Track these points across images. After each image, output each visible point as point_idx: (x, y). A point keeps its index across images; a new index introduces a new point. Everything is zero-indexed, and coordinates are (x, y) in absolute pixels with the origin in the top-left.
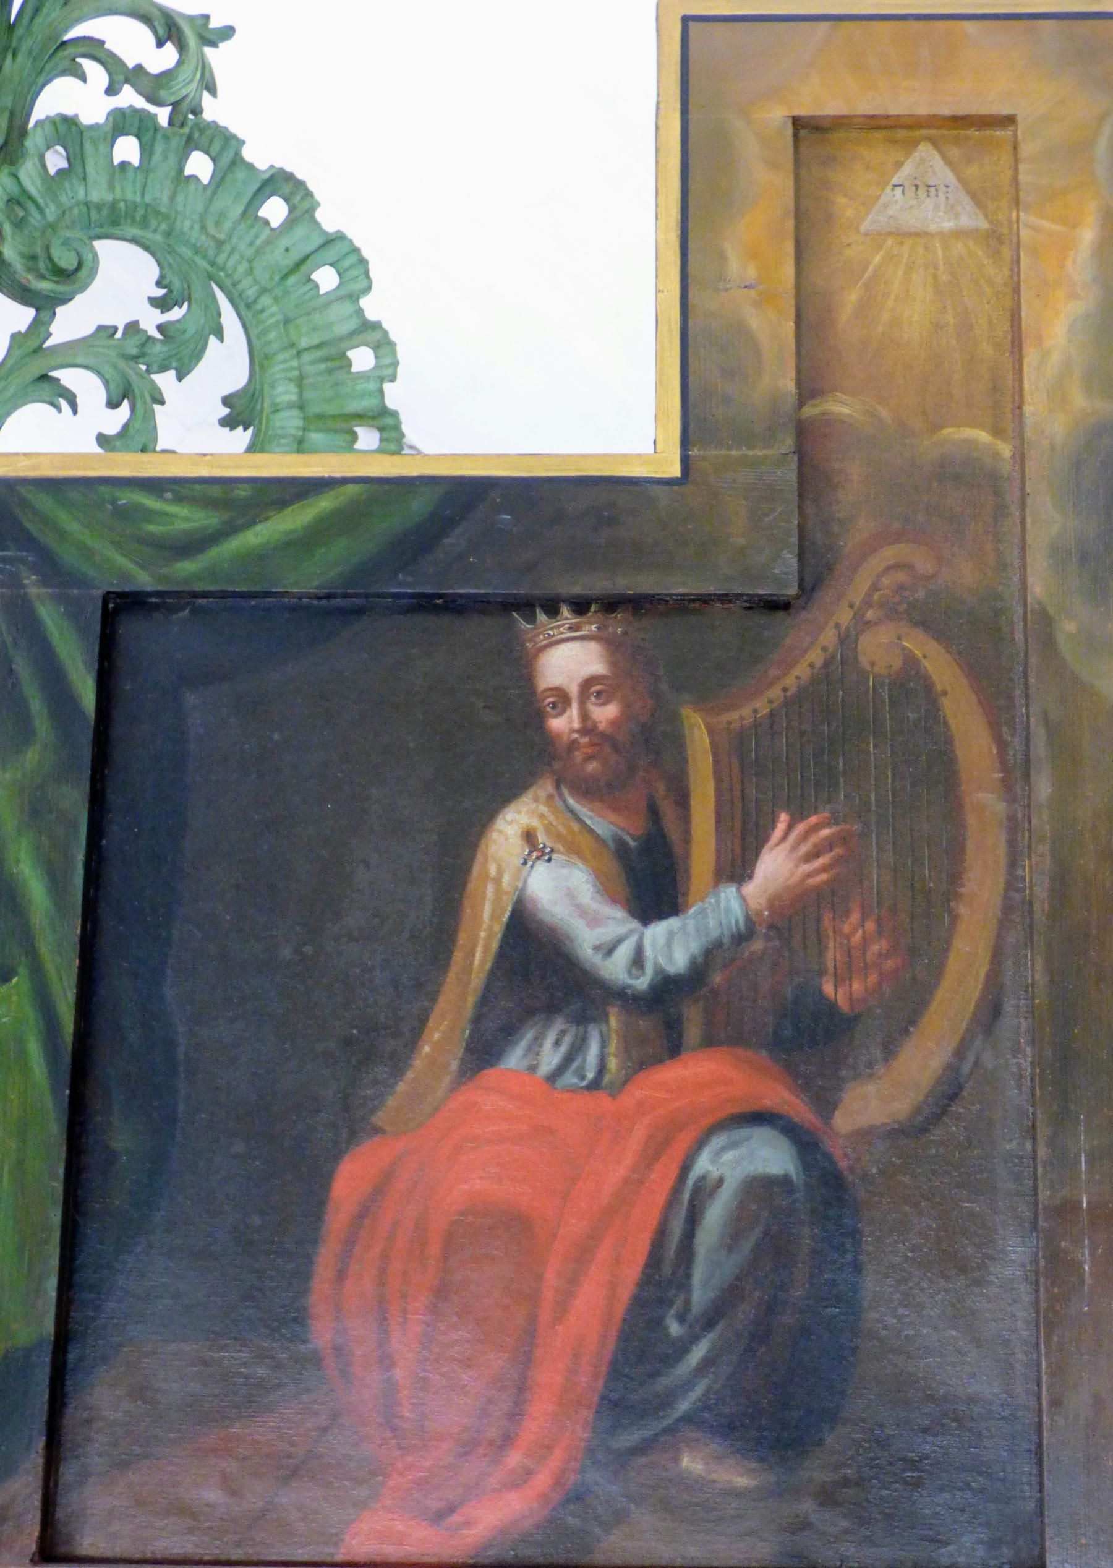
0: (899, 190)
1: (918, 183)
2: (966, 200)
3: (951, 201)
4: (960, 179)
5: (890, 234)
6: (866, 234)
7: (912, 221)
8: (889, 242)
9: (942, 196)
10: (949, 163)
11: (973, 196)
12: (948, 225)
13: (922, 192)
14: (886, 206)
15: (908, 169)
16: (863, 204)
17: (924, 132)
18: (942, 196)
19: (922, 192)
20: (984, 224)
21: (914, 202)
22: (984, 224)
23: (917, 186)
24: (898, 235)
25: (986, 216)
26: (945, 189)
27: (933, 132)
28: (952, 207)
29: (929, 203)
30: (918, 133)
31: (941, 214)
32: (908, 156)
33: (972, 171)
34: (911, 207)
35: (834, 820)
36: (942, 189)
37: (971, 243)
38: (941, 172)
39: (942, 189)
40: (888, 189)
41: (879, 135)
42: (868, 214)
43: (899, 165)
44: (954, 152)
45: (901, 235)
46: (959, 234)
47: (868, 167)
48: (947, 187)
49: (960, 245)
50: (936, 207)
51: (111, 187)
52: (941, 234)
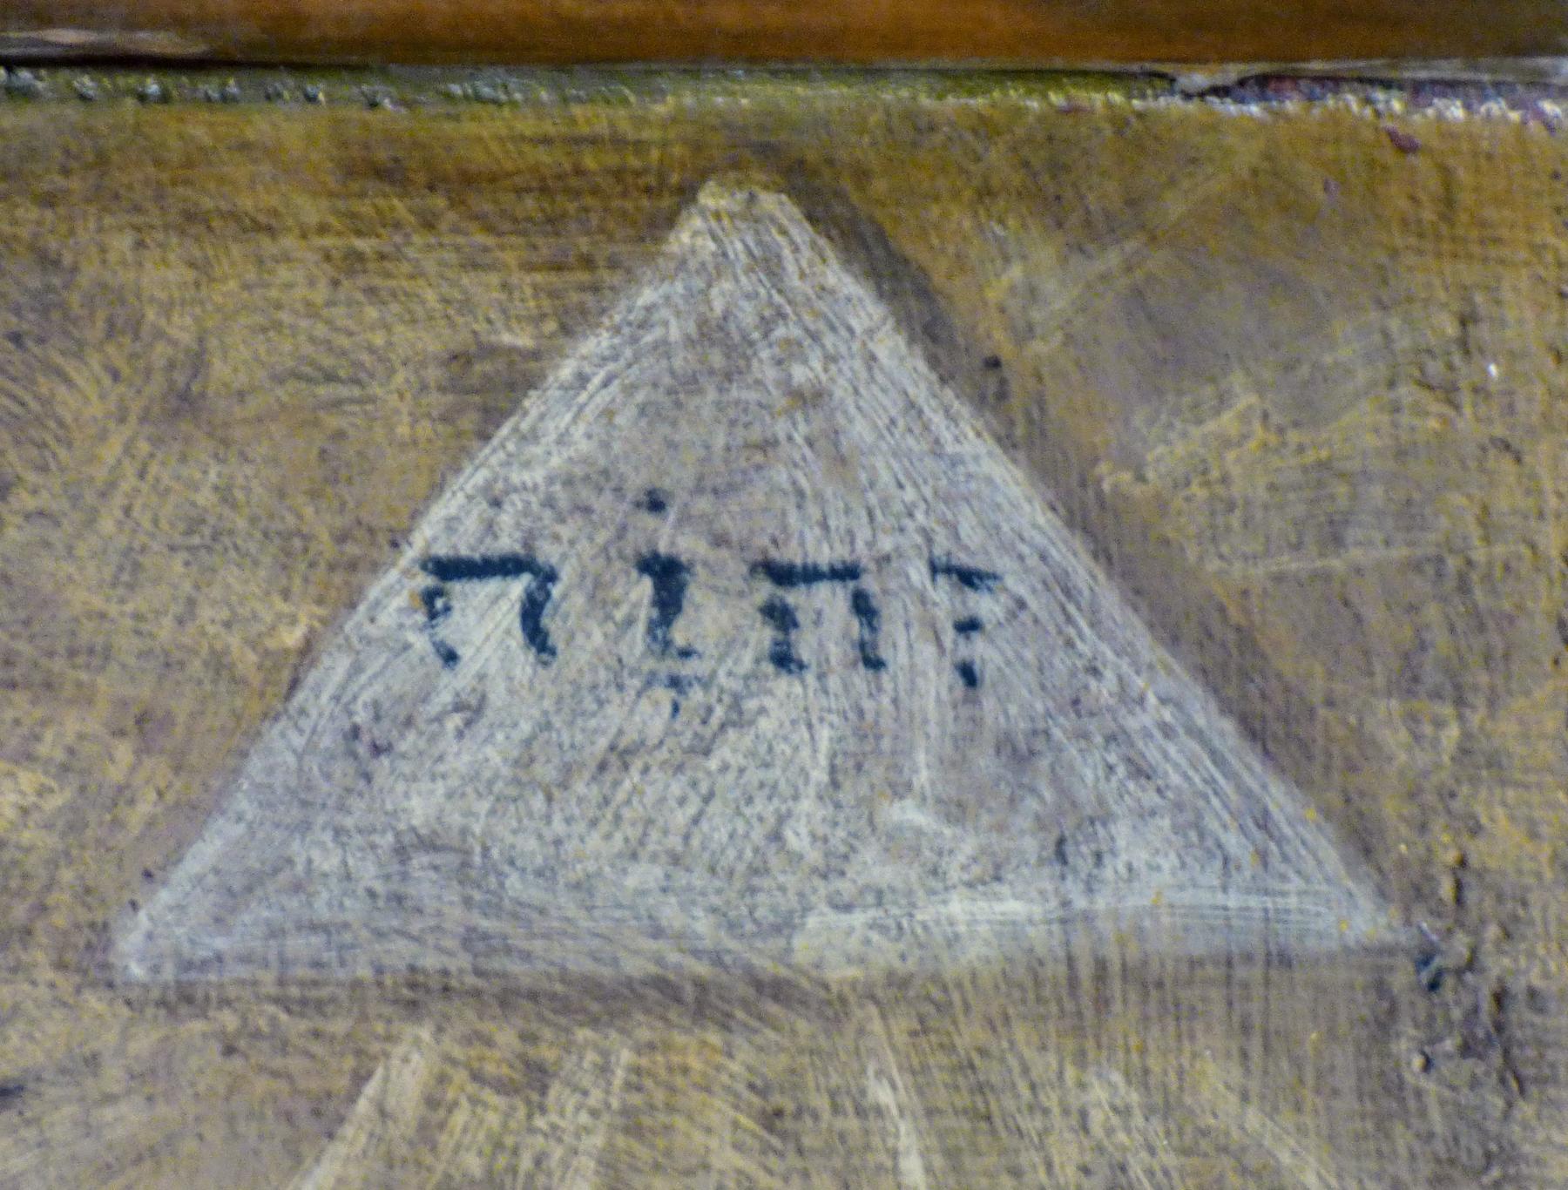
0: (487, 615)
1: (686, 544)
2: (1159, 695)
3: (1014, 702)
4: (1089, 515)
5: (417, 995)
6: (182, 999)
7: (618, 885)
8: (409, 1067)
9: (919, 663)
10: (987, 381)
11: (1227, 657)
12: (987, 916)
13: (718, 617)
14: (366, 747)
15: (567, 425)
16: (145, 725)
17: (743, 97)
18: (919, 663)
19: (718, 617)
20: (1339, 912)
21: (650, 716)
22: (1339, 912)
23: (668, 576)
24: (508, 998)
25: (1362, 841)
26: (944, 598)
27: (822, 98)
28: (1018, 754)
29: (796, 723)
30: (671, 105)
31: (907, 814)
32: (571, 323)
33: (1207, 446)
34: (622, 754)
35: (85, 220)
36: (915, 606)
37: (1214, 1082)
38: (883, 434)
39: (915, 606)
40: (394, 591)
41: (293, 122)
42: (192, 814)
43: (487, 390)
44: (1026, 282)
45: (531, 1005)
46: (1087, 992)
47: (183, 405)
48: (968, 578)
49: (1104, 1090)
50: (865, 759)
51: (412, 426)
52: (922, 999)
